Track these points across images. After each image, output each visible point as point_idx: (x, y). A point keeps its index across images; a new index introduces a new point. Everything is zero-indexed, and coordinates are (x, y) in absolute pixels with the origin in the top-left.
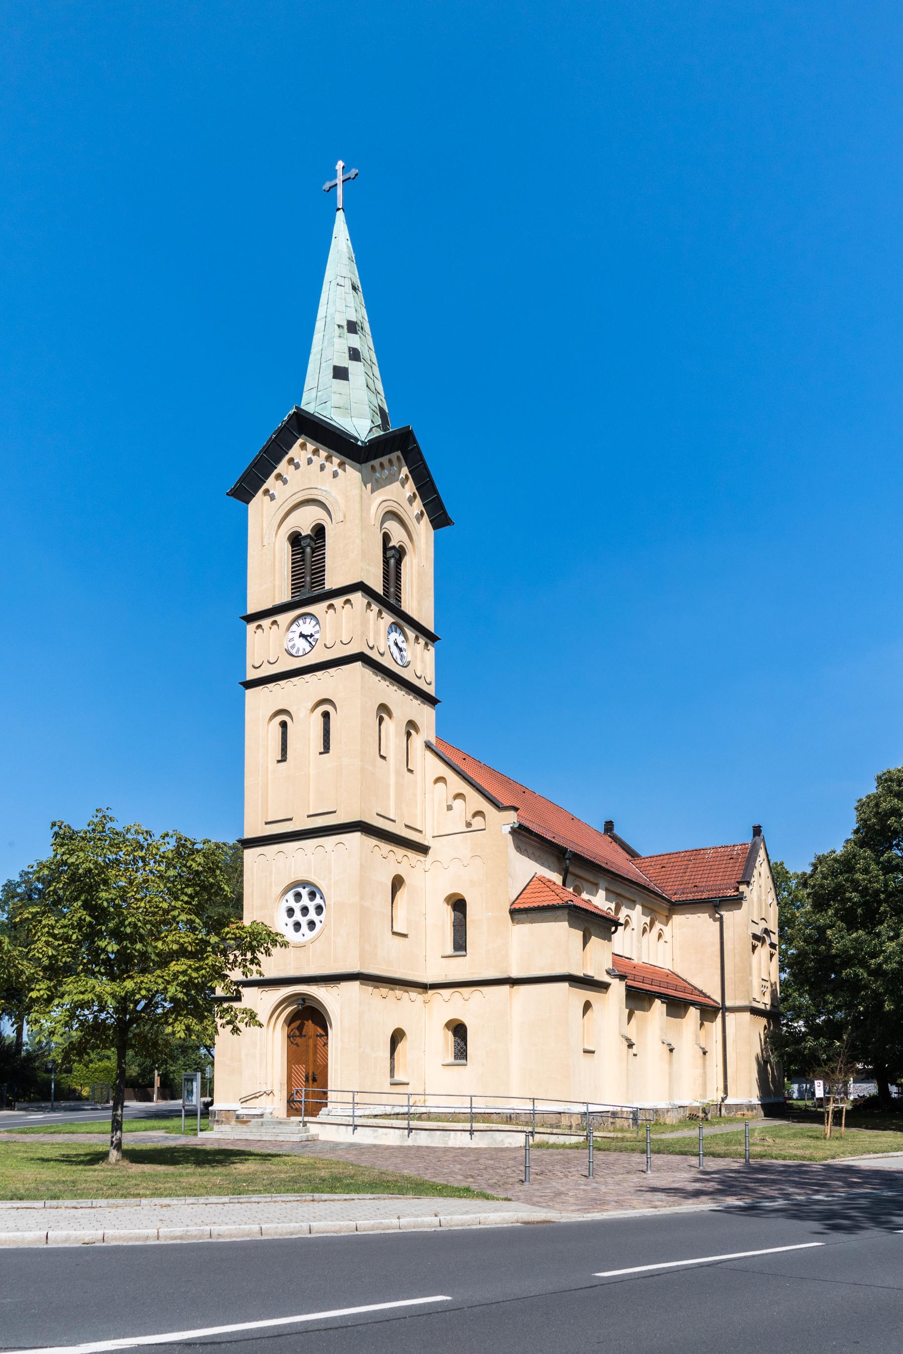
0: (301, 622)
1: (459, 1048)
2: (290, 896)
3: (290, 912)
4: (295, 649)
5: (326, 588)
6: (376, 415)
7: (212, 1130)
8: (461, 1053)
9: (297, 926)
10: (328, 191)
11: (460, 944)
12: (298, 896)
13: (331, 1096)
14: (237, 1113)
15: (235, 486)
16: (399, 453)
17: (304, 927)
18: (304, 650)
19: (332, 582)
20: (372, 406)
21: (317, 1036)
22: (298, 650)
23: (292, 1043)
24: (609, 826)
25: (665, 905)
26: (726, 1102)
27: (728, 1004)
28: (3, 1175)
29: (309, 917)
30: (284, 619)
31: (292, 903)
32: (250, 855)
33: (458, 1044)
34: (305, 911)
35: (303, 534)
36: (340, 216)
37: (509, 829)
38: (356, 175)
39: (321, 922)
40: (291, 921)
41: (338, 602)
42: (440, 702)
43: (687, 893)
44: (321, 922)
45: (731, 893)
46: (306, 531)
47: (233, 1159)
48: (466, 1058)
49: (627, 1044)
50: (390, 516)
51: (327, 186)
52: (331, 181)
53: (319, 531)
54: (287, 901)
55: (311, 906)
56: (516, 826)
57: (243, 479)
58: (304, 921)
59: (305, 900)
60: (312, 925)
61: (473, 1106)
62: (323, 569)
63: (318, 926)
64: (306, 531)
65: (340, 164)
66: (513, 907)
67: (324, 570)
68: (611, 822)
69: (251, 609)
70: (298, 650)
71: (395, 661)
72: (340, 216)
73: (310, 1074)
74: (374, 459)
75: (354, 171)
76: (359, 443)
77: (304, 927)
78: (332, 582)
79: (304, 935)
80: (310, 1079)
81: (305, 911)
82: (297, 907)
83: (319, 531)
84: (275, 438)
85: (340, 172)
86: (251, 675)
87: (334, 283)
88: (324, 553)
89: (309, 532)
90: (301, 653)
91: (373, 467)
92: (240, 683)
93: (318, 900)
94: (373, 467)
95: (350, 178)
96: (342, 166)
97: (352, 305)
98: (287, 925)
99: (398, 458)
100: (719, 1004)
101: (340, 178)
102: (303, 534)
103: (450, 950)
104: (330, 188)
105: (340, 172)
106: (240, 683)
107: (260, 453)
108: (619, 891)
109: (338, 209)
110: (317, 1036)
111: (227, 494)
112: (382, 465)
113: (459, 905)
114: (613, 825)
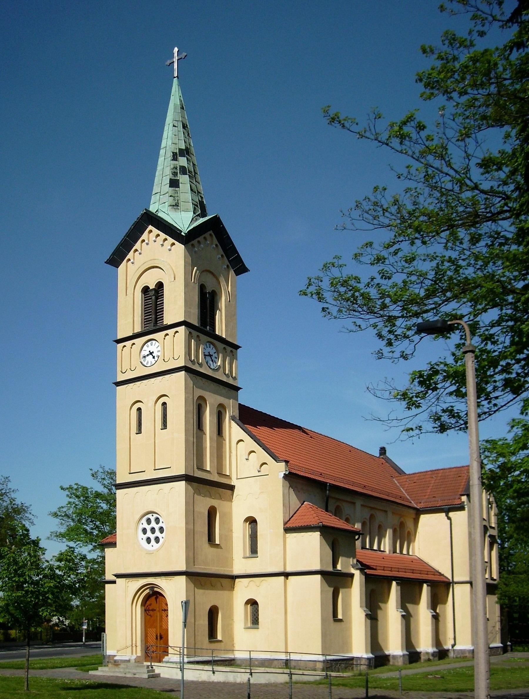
0: (149, 343)
1: (255, 617)
2: (144, 520)
3: (144, 531)
4: (146, 362)
5: (164, 324)
6: (196, 207)
7: (97, 669)
8: (255, 621)
9: (149, 540)
10: (169, 65)
11: (254, 550)
12: (149, 521)
13: (170, 650)
14: (116, 658)
15: (110, 258)
16: (211, 232)
17: (153, 541)
18: (151, 362)
19: (168, 320)
20: (194, 202)
21: (162, 610)
22: (148, 363)
23: (148, 614)
24: (383, 451)
25: (412, 512)
26: (455, 648)
27: (456, 580)
28: (4, 679)
29: (151, 526)
30: (139, 341)
31: (146, 525)
32: (120, 494)
33: (255, 615)
34: (153, 530)
35: (151, 288)
36: (175, 80)
37: (283, 475)
38: (186, 56)
39: (163, 538)
40: (145, 537)
41: (171, 332)
42: (241, 388)
43: (428, 502)
44: (163, 538)
45: (457, 502)
46: (152, 286)
47: (80, 687)
48: (258, 624)
49: (365, 614)
50: (204, 273)
51: (168, 62)
52: (170, 60)
53: (160, 285)
54: (142, 524)
55: (157, 527)
56: (287, 473)
57: (114, 254)
58: (152, 537)
59: (153, 524)
60: (157, 540)
61: (196, 648)
62: (162, 310)
63: (161, 540)
64: (152, 286)
65: (176, 50)
66: (286, 526)
67: (163, 311)
68: (384, 448)
69: (120, 337)
70: (148, 363)
71: (209, 367)
72: (175, 80)
73: (159, 635)
74: (193, 240)
75: (184, 54)
76: (183, 234)
77: (153, 541)
78: (168, 320)
79: (152, 546)
80: (159, 637)
81: (153, 530)
82: (148, 528)
83: (160, 285)
84: (133, 228)
85: (176, 55)
86: (121, 378)
87: (171, 125)
88: (163, 300)
89: (154, 287)
90: (149, 365)
91: (193, 245)
92: (114, 383)
93: (161, 524)
94: (193, 245)
95: (182, 58)
96: (177, 50)
97: (183, 138)
98: (142, 539)
99: (211, 235)
100: (449, 579)
101: (175, 59)
102: (151, 288)
103: (248, 553)
104: (170, 64)
105: (176, 55)
106: (114, 383)
107: (124, 237)
108: (372, 506)
109: (175, 77)
110: (162, 610)
111: (105, 262)
112: (199, 242)
113: (252, 521)
114: (385, 450)
